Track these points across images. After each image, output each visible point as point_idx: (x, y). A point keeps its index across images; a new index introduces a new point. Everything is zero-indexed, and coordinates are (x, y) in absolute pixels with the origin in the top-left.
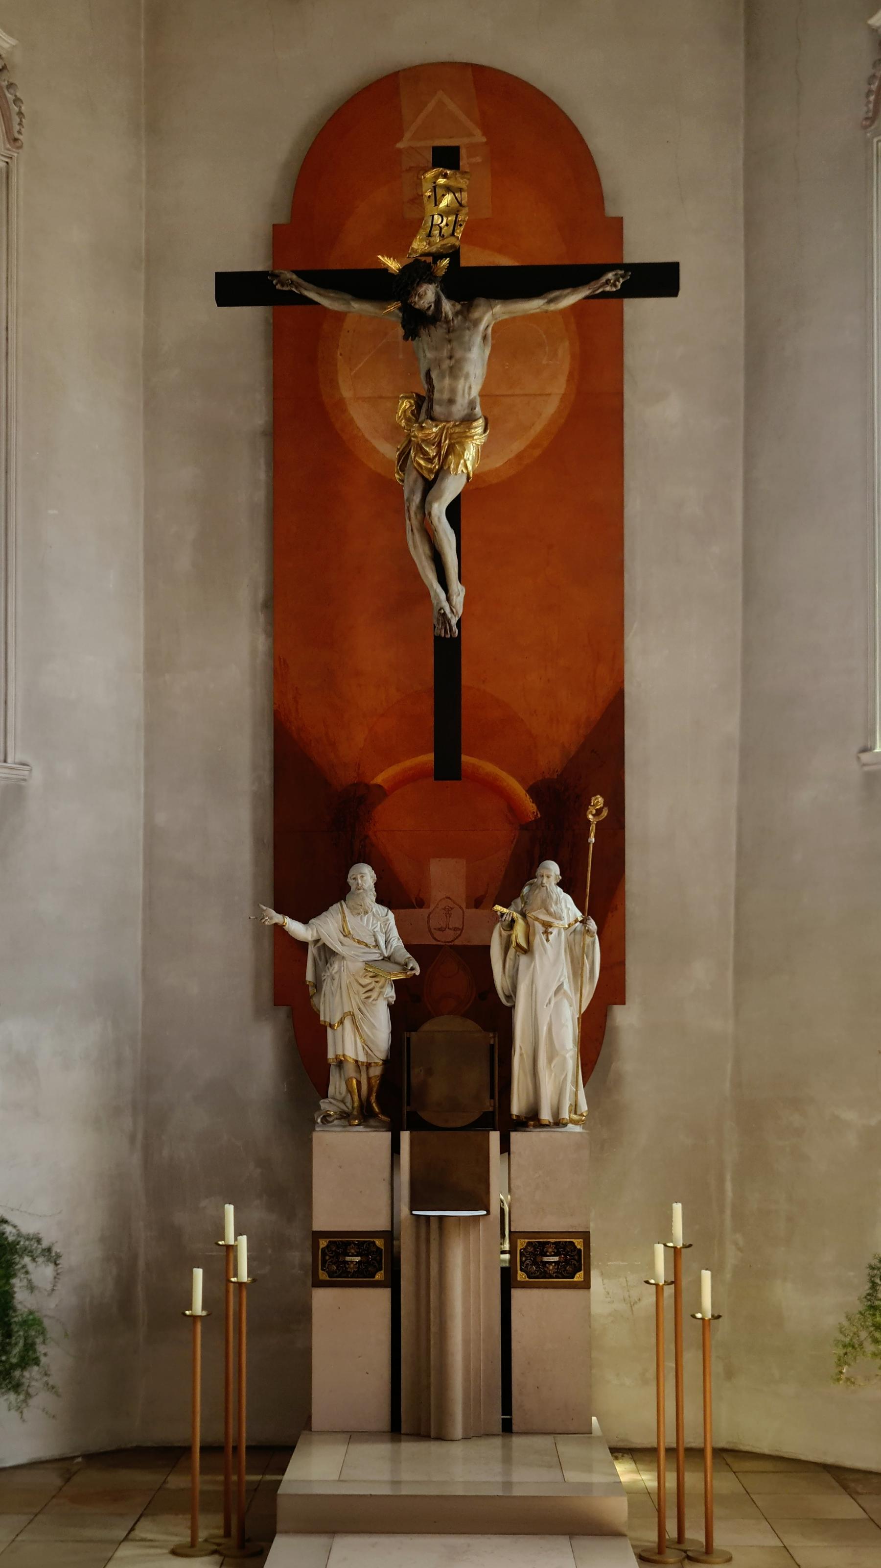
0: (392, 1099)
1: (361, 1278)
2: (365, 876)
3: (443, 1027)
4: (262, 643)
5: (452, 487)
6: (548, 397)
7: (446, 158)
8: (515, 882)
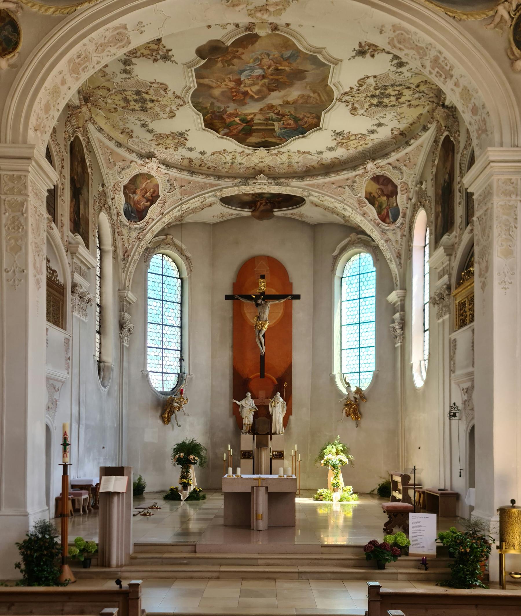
0: (253, 430)
1: (248, 458)
2: (249, 394)
3: (262, 418)
4: (231, 353)
5: (263, 332)
6: (280, 313)
7: (263, 277)
8: (273, 396)
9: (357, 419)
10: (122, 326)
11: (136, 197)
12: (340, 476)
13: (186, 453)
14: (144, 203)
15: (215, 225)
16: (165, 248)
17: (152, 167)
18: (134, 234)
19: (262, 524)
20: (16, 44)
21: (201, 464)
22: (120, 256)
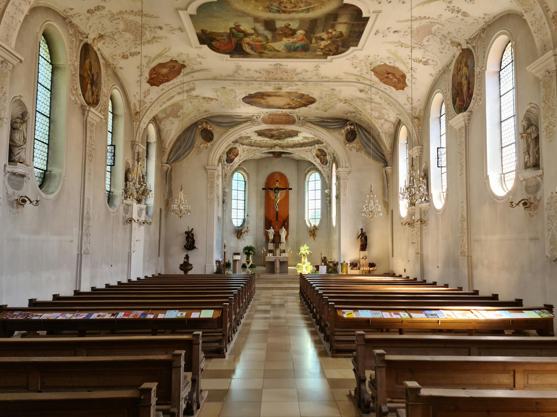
0: (273, 241)
7: (277, 181)
8: (281, 228)
10: (223, 202)
11: (230, 155)
12: (306, 259)
13: (248, 251)
18: (229, 168)
19: (278, 271)
21: (254, 255)
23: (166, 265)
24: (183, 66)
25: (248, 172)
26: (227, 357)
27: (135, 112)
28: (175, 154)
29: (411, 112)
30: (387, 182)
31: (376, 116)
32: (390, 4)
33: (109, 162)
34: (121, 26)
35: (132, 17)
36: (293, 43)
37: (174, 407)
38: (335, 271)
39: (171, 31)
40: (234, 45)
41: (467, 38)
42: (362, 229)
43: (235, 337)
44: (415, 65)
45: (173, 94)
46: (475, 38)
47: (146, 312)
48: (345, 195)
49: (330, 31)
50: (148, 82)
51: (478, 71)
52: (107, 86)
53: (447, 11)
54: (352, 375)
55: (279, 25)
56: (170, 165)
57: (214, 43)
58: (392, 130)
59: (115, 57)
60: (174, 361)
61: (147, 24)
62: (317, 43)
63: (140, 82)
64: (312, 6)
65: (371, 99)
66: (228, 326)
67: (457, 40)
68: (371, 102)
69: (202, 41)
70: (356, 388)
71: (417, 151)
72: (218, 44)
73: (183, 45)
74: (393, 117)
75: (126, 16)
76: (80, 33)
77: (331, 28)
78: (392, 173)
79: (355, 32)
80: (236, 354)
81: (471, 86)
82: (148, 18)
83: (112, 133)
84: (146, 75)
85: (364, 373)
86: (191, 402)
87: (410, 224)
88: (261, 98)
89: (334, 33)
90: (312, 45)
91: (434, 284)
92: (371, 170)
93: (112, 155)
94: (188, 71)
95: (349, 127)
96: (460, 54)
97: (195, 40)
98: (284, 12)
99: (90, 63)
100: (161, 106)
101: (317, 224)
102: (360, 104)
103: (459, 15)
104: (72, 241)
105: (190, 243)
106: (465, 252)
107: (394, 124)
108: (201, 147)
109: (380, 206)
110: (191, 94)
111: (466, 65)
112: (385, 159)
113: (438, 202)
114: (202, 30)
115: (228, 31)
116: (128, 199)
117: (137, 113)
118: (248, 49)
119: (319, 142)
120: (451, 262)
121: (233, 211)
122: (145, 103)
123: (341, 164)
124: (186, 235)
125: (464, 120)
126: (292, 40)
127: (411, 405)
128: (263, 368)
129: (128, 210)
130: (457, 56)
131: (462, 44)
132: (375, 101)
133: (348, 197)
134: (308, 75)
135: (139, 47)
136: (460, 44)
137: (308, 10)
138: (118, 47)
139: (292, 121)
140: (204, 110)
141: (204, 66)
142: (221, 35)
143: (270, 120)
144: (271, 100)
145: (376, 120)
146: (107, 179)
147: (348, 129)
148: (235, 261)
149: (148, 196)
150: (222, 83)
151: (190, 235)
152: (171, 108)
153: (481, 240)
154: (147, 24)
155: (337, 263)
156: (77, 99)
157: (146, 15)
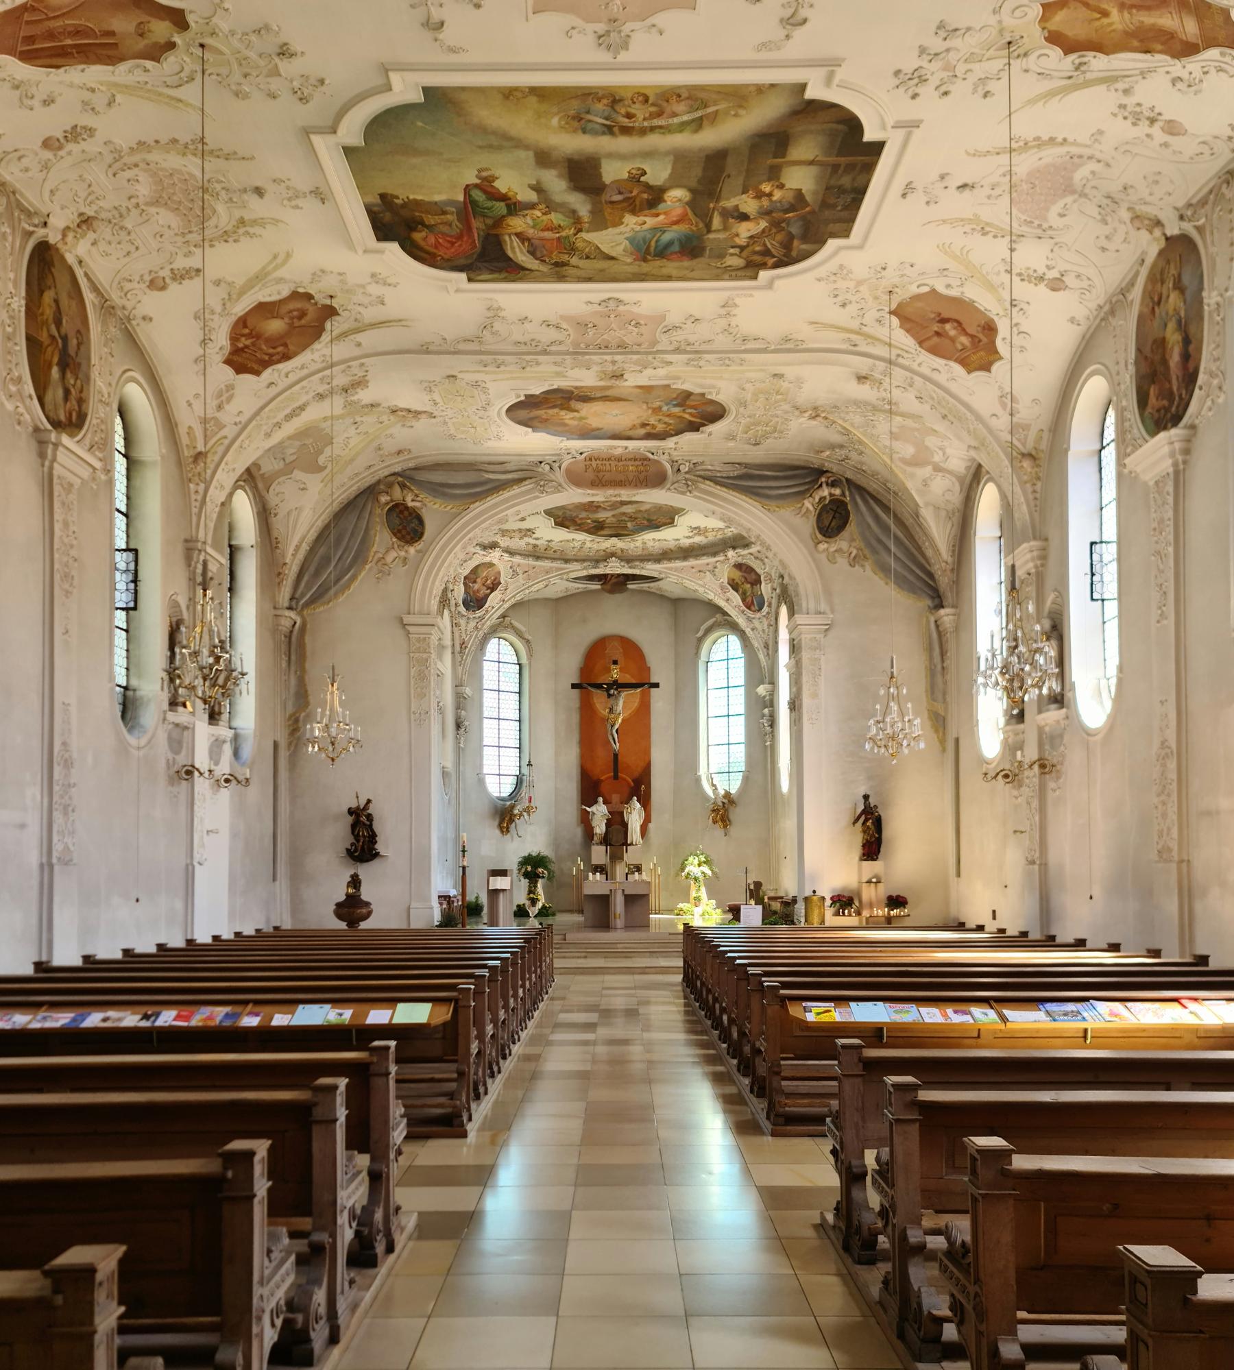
0: (606, 840)
2: (601, 799)
6: (635, 703)
7: (615, 662)
9: (725, 827)
10: (458, 726)
11: (476, 587)
12: (703, 889)
13: (533, 867)
14: (484, 591)
15: (558, 600)
16: (502, 632)
17: (494, 556)
18: (473, 624)
19: (620, 923)
20: (422, 534)
21: (549, 879)
22: (458, 648)
23: (296, 904)
24: (331, 312)
25: (527, 636)
26: (472, 1136)
27: (193, 452)
28: (316, 577)
29: (1009, 438)
30: (943, 654)
31: (908, 457)
32: (945, 98)
33: (122, 598)
34: (144, 190)
35: (173, 161)
36: (654, 229)
37: (322, 1228)
38: (788, 919)
39: (290, 199)
40: (476, 241)
41: (1181, 203)
42: (866, 797)
43: (495, 1087)
44: (1023, 290)
45: (303, 399)
46: (1203, 202)
47: (238, 1009)
48: (815, 695)
49: (766, 187)
50: (228, 362)
51: (1213, 301)
52: (109, 377)
53: (1120, 117)
54: (830, 1178)
55: (613, 172)
56: (300, 613)
57: (418, 236)
58: (956, 498)
59: (128, 286)
60: (315, 1104)
61: (219, 182)
62: (726, 228)
63: (201, 359)
64: (710, 110)
65: (890, 403)
66: (474, 1047)
67: (1151, 211)
68: (890, 412)
69: (383, 231)
70: (838, 1203)
71: (1029, 556)
72: (432, 240)
73: (330, 248)
74: (957, 459)
75: (154, 157)
76: (23, 210)
77: (769, 180)
78: (957, 629)
79: (841, 190)
80: (500, 1128)
81: (1191, 348)
82: (221, 163)
83: (126, 515)
84: (222, 340)
85: (862, 1156)
86: (370, 1232)
87: (1010, 776)
88: (562, 407)
89: (777, 195)
90: (711, 236)
91: (1080, 944)
92: (895, 615)
93: (131, 577)
94: (346, 327)
95: (825, 492)
96: (1161, 253)
97: (362, 226)
98: (626, 131)
99: (56, 301)
100: (268, 435)
101: (735, 786)
102: (858, 419)
103: (1156, 130)
104: (23, 826)
105: (363, 842)
106: (1170, 850)
107: (961, 480)
108: (389, 558)
109: (917, 721)
110: (355, 398)
111: (1179, 287)
112: (935, 586)
113: (1093, 705)
114: (383, 196)
115: (461, 198)
116: (181, 709)
117: (199, 456)
118: (519, 254)
119: (739, 542)
120: (1133, 882)
121: (486, 750)
122: (221, 426)
123: (804, 605)
124: (350, 819)
125: (1172, 454)
126: (651, 222)
127: (984, 1196)
128: (575, 1161)
129: (180, 743)
130: (1150, 260)
131: (1164, 221)
132: (903, 408)
133: (823, 702)
134: (701, 332)
135: (198, 251)
136: (1158, 223)
137: (698, 125)
138: (135, 255)
139: (652, 476)
140: (394, 449)
141: (392, 309)
142: (439, 209)
143: (590, 475)
144: (594, 414)
145: (909, 469)
146: (117, 650)
147: (822, 499)
148: (494, 894)
149: (237, 690)
150: (450, 365)
151: (364, 819)
152: (298, 443)
153: (1218, 813)
154: (219, 182)
155: (794, 900)
156: (21, 410)
157: (216, 154)
